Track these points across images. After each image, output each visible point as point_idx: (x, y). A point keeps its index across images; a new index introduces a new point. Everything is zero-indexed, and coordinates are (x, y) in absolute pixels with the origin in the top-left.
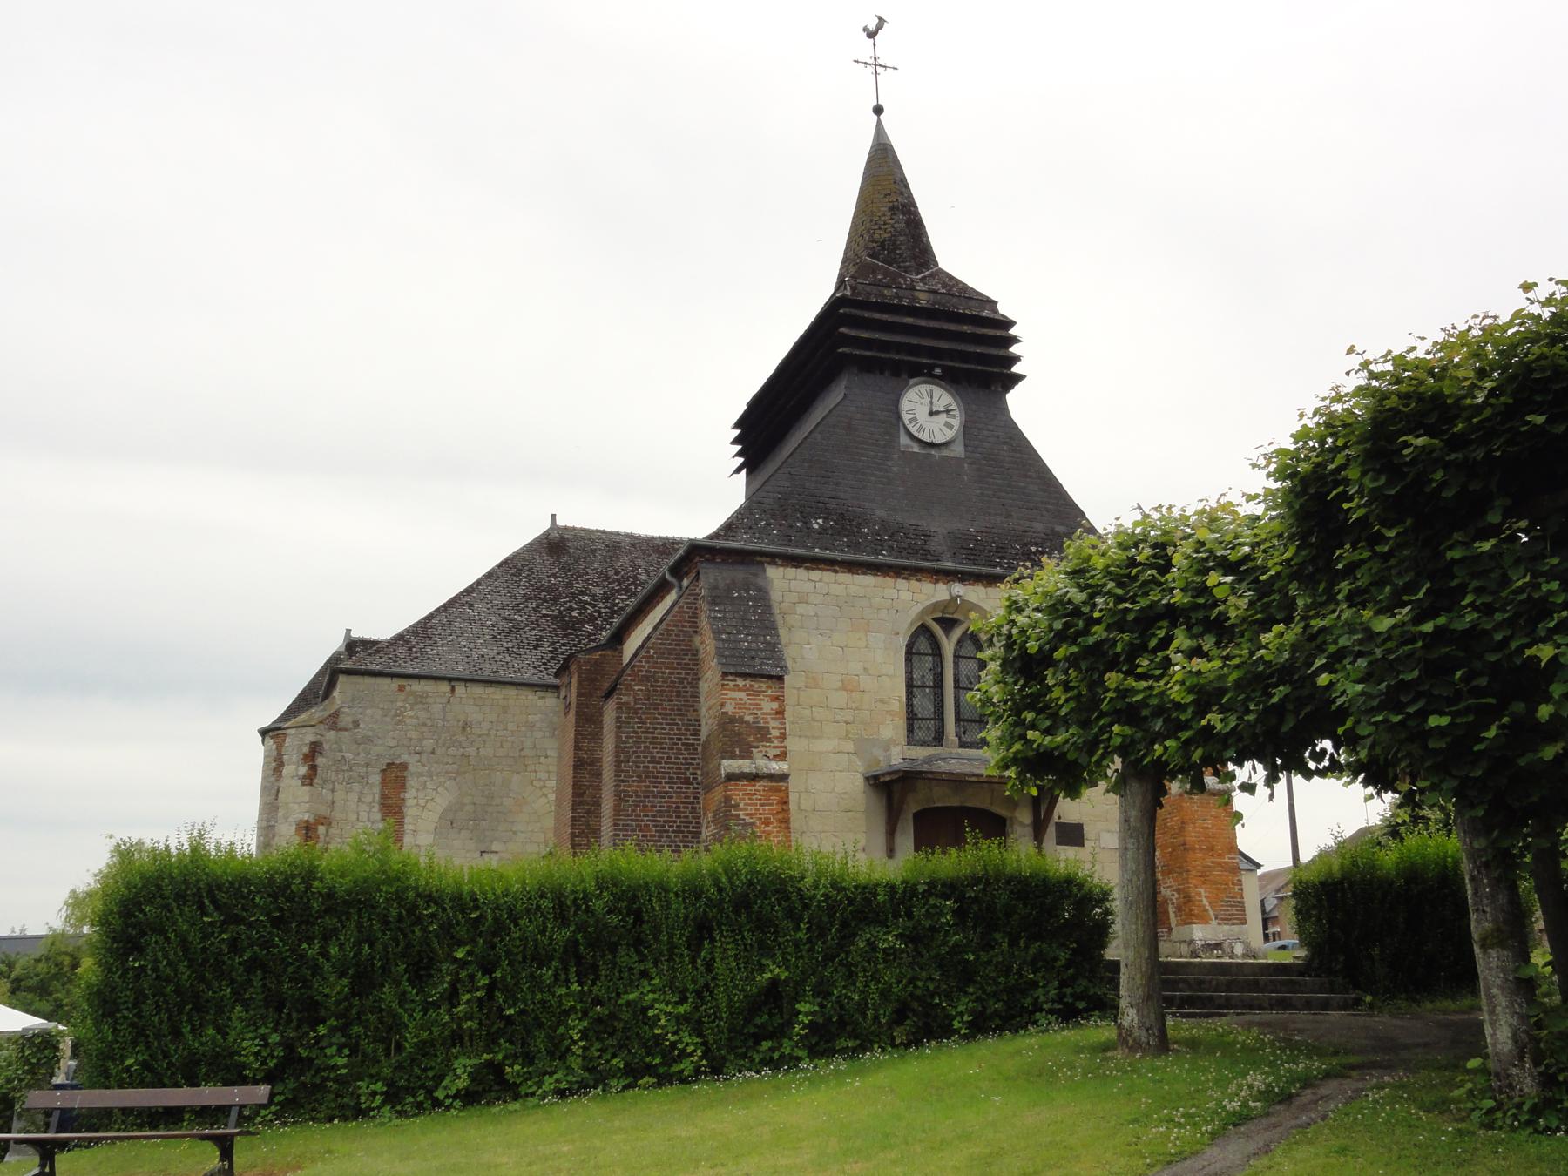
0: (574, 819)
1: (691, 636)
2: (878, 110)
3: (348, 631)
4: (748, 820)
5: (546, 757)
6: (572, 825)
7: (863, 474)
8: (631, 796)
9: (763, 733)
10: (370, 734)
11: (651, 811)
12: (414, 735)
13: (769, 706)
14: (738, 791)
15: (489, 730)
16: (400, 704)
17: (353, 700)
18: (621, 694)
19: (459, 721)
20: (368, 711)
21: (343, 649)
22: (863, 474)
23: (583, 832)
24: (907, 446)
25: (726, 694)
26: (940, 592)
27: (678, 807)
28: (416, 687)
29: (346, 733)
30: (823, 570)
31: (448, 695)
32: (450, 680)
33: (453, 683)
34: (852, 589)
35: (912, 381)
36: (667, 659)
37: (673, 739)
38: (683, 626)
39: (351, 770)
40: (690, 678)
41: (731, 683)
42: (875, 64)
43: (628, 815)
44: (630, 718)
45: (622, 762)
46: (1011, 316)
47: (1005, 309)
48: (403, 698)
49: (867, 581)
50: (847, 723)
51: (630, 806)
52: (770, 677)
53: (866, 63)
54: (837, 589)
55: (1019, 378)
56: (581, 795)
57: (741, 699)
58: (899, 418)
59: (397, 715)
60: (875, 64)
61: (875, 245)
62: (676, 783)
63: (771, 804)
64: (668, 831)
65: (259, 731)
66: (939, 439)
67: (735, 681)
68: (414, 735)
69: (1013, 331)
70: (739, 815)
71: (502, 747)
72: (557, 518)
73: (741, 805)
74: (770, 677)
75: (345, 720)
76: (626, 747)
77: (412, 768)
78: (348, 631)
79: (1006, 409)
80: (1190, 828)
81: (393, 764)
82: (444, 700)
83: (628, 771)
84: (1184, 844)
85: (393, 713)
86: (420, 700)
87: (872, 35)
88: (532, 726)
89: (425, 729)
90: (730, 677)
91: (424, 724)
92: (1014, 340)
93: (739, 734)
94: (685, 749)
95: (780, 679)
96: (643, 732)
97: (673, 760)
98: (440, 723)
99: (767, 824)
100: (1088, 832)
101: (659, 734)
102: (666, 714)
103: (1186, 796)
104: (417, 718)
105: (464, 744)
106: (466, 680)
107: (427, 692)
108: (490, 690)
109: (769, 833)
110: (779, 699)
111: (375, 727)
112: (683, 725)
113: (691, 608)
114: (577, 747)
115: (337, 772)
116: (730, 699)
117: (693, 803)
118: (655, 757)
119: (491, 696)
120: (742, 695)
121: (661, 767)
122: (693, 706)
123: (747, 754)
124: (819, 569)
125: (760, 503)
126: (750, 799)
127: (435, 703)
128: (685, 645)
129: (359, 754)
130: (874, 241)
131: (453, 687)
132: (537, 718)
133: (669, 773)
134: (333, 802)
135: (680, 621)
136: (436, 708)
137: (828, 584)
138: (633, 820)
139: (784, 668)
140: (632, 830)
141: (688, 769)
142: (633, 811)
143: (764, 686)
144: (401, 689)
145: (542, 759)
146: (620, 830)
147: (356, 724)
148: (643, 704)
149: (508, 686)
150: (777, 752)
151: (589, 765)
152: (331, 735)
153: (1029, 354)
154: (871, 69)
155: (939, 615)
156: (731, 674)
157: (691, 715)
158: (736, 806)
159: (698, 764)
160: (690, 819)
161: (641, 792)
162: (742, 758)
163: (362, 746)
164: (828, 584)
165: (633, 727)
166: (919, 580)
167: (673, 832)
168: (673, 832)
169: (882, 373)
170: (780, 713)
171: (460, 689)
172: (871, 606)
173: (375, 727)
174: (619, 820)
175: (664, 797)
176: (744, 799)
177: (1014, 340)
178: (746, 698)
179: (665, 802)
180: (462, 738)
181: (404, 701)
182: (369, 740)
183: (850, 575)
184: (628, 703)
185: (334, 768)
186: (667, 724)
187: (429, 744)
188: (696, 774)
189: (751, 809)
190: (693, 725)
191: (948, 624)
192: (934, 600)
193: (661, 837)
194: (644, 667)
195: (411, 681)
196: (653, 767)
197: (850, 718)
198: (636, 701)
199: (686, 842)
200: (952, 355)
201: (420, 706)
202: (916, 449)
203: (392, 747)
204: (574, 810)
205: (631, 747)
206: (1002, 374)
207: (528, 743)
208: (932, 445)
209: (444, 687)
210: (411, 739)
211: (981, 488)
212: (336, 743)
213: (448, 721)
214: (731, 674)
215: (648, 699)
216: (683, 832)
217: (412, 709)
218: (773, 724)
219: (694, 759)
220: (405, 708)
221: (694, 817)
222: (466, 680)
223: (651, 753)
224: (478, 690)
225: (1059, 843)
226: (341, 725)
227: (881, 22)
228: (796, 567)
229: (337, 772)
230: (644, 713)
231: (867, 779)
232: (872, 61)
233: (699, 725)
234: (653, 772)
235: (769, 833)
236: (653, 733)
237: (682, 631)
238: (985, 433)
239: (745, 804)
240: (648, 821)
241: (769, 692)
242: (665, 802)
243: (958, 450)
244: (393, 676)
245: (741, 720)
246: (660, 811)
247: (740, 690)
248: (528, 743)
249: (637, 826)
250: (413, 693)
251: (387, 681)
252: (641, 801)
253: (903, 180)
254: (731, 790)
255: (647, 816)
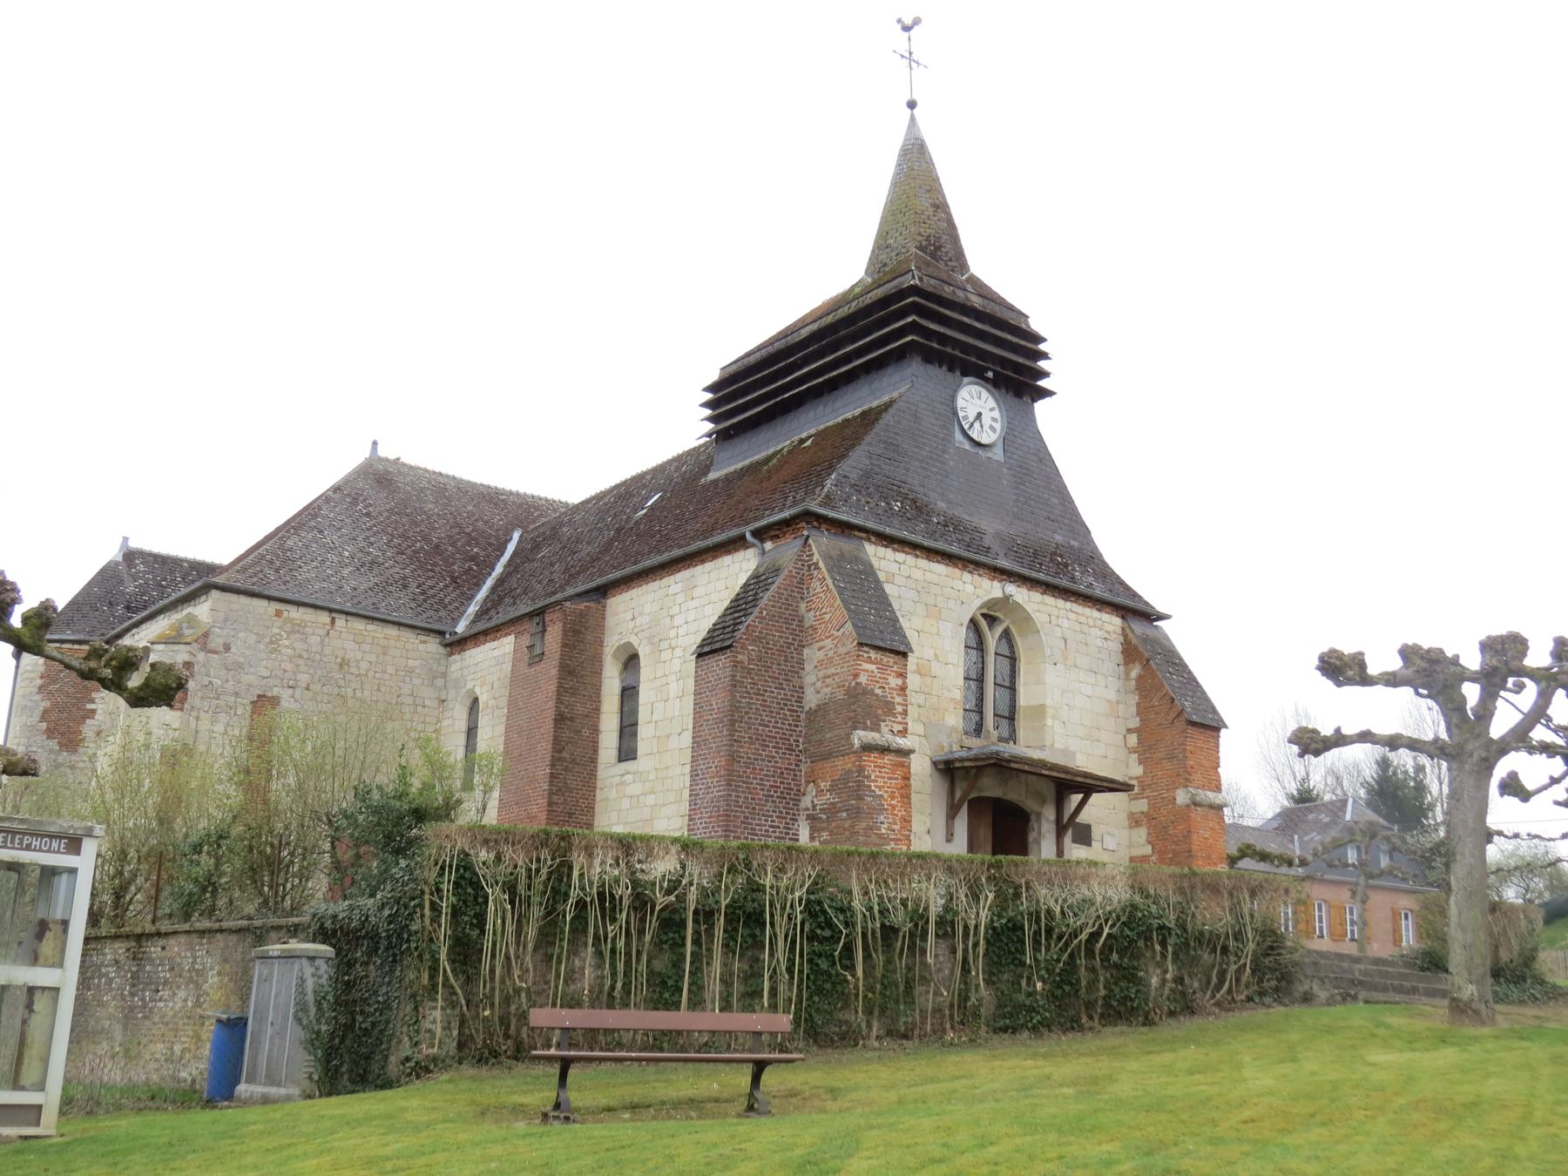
0: (552, 776)
1: (798, 602)
2: (912, 105)
3: (126, 539)
4: (878, 792)
5: (424, 706)
6: (550, 782)
7: (927, 463)
8: (743, 757)
9: (889, 708)
10: (242, 660)
11: (759, 774)
12: (288, 666)
13: (895, 682)
14: (871, 761)
15: (367, 671)
16: (276, 631)
17: (226, 620)
18: (737, 652)
19: (336, 657)
20: (241, 635)
21: (120, 559)
22: (927, 463)
23: (560, 790)
24: (961, 443)
25: (860, 665)
26: (993, 589)
27: (782, 773)
28: (295, 613)
29: (215, 656)
30: (907, 553)
31: (328, 627)
32: (331, 610)
33: (334, 615)
34: (929, 576)
35: (966, 380)
36: (778, 622)
37: (779, 704)
38: (792, 591)
39: (218, 698)
40: (796, 643)
41: (866, 655)
42: (910, 57)
43: (740, 776)
44: (745, 677)
45: (736, 721)
46: (1042, 333)
47: (1036, 325)
48: (279, 624)
49: (940, 569)
50: (919, 706)
51: (741, 767)
52: (897, 653)
53: (902, 56)
54: (917, 574)
55: (1046, 393)
56: (560, 751)
57: (873, 672)
58: (955, 413)
59: (271, 642)
60: (910, 57)
61: (920, 238)
62: (781, 748)
63: (897, 779)
64: (773, 796)
65: (1362, 654)
66: (985, 440)
67: (868, 653)
68: (288, 666)
69: (1042, 347)
70: (870, 786)
71: (379, 690)
72: (379, 447)
73: (873, 777)
74: (897, 653)
75: (216, 642)
76: (739, 707)
77: (284, 703)
78: (126, 539)
79: (1034, 420)
80: (1194, 836)
81: (264, 696)
82: (323, 632)
83: (740, 732)
84: (1190, 851)
85: (268, 640)
86: (297, 629)
87: (907, 29)
88: (410, 672)
89: (300, 661)
90: (865, 649)
91: (300, 656)
92: (1044, 356)
93: (871, 707)
94: (791, 715)
95: (904, 655)
96: (755, 694)
97: (779, 725)
98: (317, 657)
99: (893, 798)
100: (1096, 833)
101: (769, 697)
102: (775, 678)
103: (1193, 807)
104: (294, 650)
105: (342, 683)
106: (347, 613)
107: (305, 622)
108: (371, 627)
109: (894, 807)
110: (902, 675)
111: (247, 653)
112: (789, 690)
113: (799, 573)
114: (559, 701)
115: (202, 698)
116: (863, 670)
117: (794, 770)
118: (764, 720)
119: (371, 634)
120: (873, 667)
121: (769, 731)
122: (798, 673)
123: (876, 728)
124: (903, 552)
125: (846, 477)
126: (880, 772)
127: (313, 634)
128: (793, 610)
129: (227, 681)
130: (920, 234)
131: (333, 619)
132: (417, 663)
133: (776, 738)
134: (197, 732)
135: (788, 585)
136: (314, 640)
137: (910, 567)
138: (744, 782)
139: (908, 645)
140: (743, 792)
141: (792, 735)
142: (745, 772)
143: (892, 660)
144: (278, 614)
145: (420, 709)
146: (733, 790)
147: (227, 648)
148: (755, 665)
149: (390, 626)
150: (900, 727)
151: (569, 720)
152: (201, 656)
153: (1058, 370)
154: (906, 62)
155: (985, 611)
156: (867, 645)
157: (796, 681)
158: (868, 777)
159: (801, 732)
160: (792, 786)
161: (752, 754)
162: (872, 730)
163: (232, 673)
164: (910, 567)
165: (746, 687)
166: (980, 575)
167: (778, 797)
168: (778, 797)
169: (940, 366)
170: (903, 689)
171: (341, 621)
172: (943, 595)
173: (247, 653)
174: (732, 780)
175: (770, 762)
176: (874, 771)
177: (1044, 356)
178: (876, 671)
179: (772, 766)
180: (338, 676)
181: (280, 628)
182: (240, 666)
183: (926, 561)
184: (743, 663)
185: (200, 694)
186: (776, 688)
187: (304, 678)
188: (798, 741)
189: (880, 782)
190: (797, 692)
191: (992, 620)
192: (990, 597)
193: (767, 801)
194: (757, 627)
195: (289, 607)
196: (762, 730)
197: (921, 702)
198: (750, 660)
199: (788, 808)
200: (1003, 362)
201: (297, 636)
202: (967, 446)
203: (264, 678)
204: (553, 766)
205: (744, 707)
206: (1027, 385)
207: (406, 689)
208: (979, 444)
209: (324, 618)
210: (285, 671)
211: (1016, 494)
212: (204, 666)
213: (325, 656)
214: (867, 645)
215: (760, 660)
216: (785, 798)
217: (288, 638)
218: (898, 699)
219: (797, 726)
220: (281, 636)
221: (795, 785)
222: (347, 613)
223: (761, 715)
224: (359, 625)
225: (1074, 841)
226: (211, 646)
227: (917, 21)
228: (886, 547)
229: (202, 698)
230: (756, 675)
231: (935, 763)
232: (907, 55)
233: (803, 693)
234: (762, 735)
235: (894, 807)
236: (763, 695)
237: (791, 596)
238: (1020, 441)
239: (876, 776)
240: (757, 784)
241: (895, 669)
242: (772, 766)
243: (998, 454)
244: (270, 598)
245: (872, 692)
246: (767, 776)
247: (872, 663)
248: (406, 689)
249: (747, 788)
250: (290, 620)
251: (264, 603)
252: (751, 763)
253: (936, 180)
254: (865, 761)
255: (756, 779)
